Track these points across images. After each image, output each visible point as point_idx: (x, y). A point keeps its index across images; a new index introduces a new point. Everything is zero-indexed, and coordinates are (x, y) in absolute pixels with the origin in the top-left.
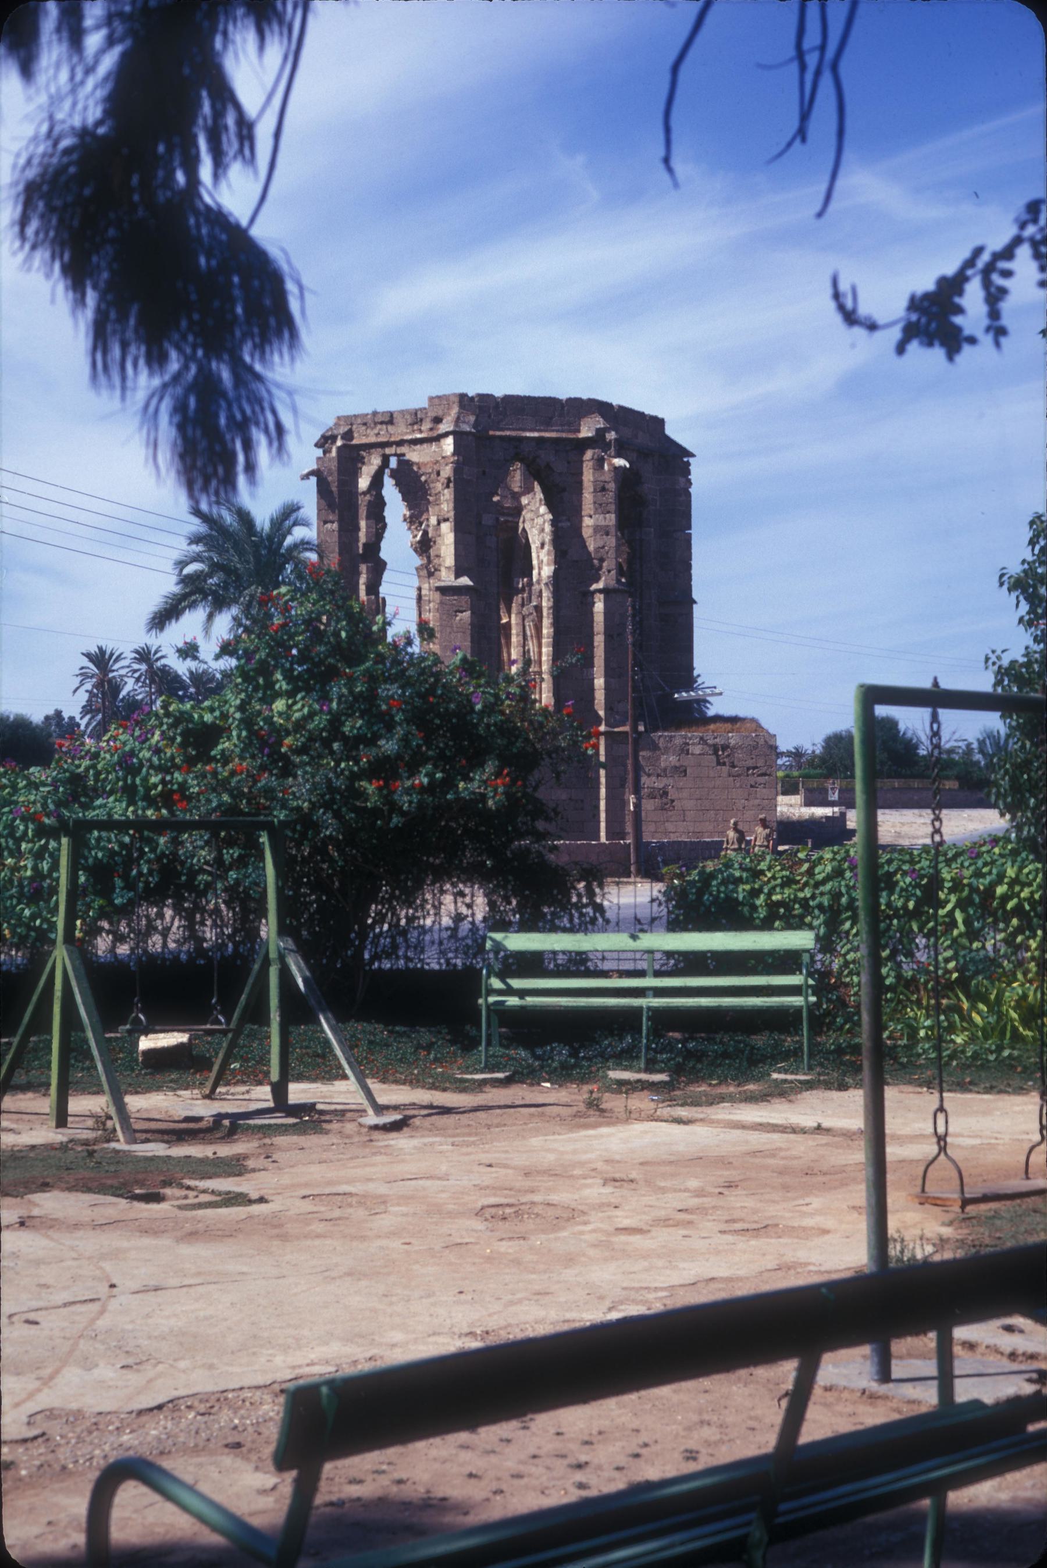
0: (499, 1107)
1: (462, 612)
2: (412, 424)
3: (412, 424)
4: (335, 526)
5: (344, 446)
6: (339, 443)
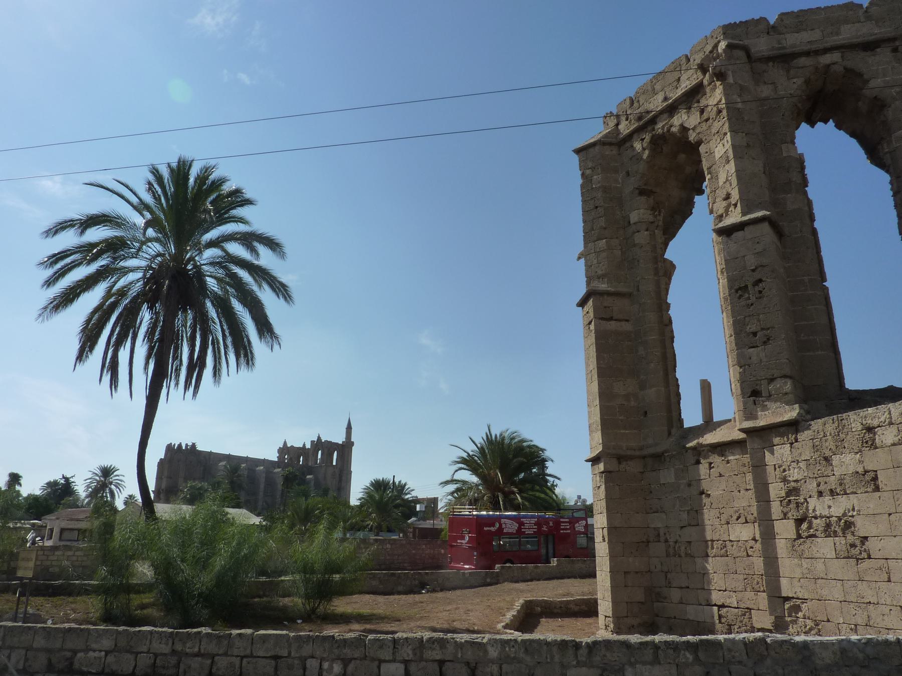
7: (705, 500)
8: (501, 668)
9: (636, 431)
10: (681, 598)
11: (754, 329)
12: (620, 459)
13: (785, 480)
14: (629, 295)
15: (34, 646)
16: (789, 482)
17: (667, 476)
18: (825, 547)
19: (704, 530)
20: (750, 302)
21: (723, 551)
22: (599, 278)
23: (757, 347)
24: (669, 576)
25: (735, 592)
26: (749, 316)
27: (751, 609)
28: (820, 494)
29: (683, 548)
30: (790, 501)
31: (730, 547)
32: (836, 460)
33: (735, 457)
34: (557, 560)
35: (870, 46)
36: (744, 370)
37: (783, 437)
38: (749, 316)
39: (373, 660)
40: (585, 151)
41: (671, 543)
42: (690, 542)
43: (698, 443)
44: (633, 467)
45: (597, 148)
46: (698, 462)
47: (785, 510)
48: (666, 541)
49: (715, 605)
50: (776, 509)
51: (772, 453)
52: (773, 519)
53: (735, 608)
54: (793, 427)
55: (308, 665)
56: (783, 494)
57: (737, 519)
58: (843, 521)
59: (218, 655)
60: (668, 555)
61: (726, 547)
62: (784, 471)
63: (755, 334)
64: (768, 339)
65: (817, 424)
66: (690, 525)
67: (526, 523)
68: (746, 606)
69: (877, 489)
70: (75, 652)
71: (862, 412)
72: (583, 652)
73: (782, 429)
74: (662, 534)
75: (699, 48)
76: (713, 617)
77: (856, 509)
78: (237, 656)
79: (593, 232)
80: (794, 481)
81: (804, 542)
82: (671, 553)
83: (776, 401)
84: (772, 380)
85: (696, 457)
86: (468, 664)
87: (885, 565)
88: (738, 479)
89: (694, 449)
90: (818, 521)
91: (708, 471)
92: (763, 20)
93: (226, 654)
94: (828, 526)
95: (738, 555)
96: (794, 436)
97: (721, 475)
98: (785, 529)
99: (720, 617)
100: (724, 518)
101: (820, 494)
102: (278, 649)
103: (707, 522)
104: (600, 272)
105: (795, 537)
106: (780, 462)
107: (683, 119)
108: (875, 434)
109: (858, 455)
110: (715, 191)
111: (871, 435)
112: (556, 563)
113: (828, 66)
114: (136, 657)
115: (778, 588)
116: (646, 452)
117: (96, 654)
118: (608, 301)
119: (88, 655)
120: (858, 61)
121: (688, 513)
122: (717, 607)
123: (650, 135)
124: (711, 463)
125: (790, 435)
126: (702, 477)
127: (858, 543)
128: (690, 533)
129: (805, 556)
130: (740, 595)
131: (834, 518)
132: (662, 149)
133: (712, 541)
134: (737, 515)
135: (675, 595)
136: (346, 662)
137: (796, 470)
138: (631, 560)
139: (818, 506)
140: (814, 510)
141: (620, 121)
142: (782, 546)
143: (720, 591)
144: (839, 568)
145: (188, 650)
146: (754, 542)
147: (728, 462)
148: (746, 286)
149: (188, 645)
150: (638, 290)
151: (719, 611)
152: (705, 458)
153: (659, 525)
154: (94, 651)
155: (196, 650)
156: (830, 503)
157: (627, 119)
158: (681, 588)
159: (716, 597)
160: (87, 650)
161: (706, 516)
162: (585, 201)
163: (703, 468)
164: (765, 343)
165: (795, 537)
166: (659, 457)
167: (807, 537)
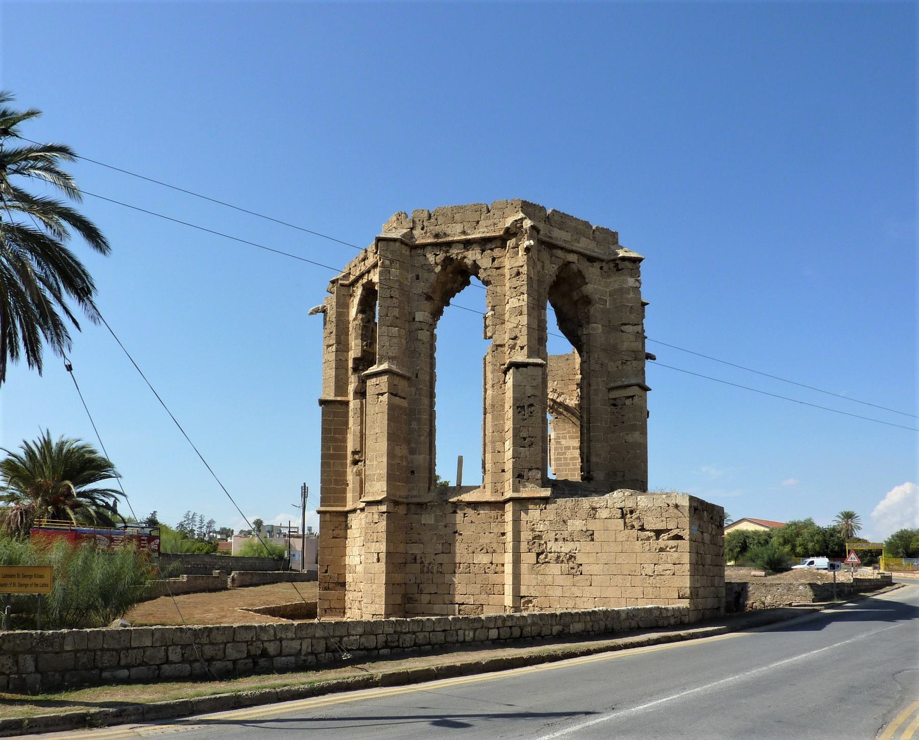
7: (458, 537)
8: (531, 628)
9: (404, 484)
10: (430, 600)
11: (525, 436)
12: (396, 503)
13: (533, 530)
14: (408, 379)
15: (317, 636)
16: (535, 531)
17: (428, 519)
19: (455, 557)
20: (524, 417)
21: (467, 570)
22: (389, 359)
23: (525, 447)
24: (421, 586)
25: (473, 595)
26: (523, 426)
27: (483, 605)
28: (556, 540)
29: (435, 568)
30: (535, 542)
31: (473, 567)
32: (570, 522)
33: (485, 512)
34: (187, 577)
35: (591, 259)
36: (516, 461)
37: (536, 505)
38: (523, 426)
39: (486, 628)
40: (386, 242)
41: (425, 565)
42: (442, 564)
43: (458, 500)
44: (402, 510)
45: (398, 244)
46: (455, 512)
47: (530, 547)
48: (422, 563)
49: (457, 604)
50: (524, 546)
51: (527, 514)
52: (521, 552)
53: (472, 605)
54: (545, 500)
55: (459, 634)
56: (531, 538)
57: (481, 551)
58: (568, 555)
59: (418, 632)
60: (422, 572)
61: (469, 567)
62: (534, 525)
63: (525, 439)
64: (532, 444)
65: (561, 501)
67: (116, 540)
68: (480, 603)
69: (592, 540)
70: (341, 637)
71: (590, 499)
72: (558, 618)
74: (418, 558)
75: (500, 207)
76: (454, 611)
77: (578, 549)
78: (427, 632)
79: (387, 318)
80: (539, 531)
81: (540, 566)
82: (425, 571)
83: (531, 483)
84: (530, 470)
85: (454, 509)
86: (520, 627)
87: (590, 578)
88: (485, 526)
89: (453, 503)
90: (552, 554)
91: (463, 518)
92: (543, 209)
93: (422, 631)
94: (558, 557)
95: (479, 572)
96: (544, 506)
97: (472, 522)
98: (528, 559)
99: (459, 610)
100: (471, 550)
101: (556, 540)
102: (445, 626)
103: (457, 551)
104: (390, 354)
105: (535, 563)
106: (532, 520)
108: (596, 511)
109: (584, 521)
110: (496, 325)
111: (594, 512)
112: (186, 579)
113: (570, 262)
114: (376, 637)
115: (519, 591)
116: (411, 500)
117: (355, 637)
118: (397, 380)
119: (350, 639)
120: (585, 267)
121: (442, 545)
122: (458, 605)
123: (444, 255)
124: (465, 514)
125: (541, 505)
127: (576, 567)
128: (444, 558)
129: (540, 573)
130: (476, 597)
131: (562, 553)
132: (446, 268)
134: (481, 548)
135: (425, 598)
136: (475, 630)
137: (542, 525)
138: (396, 575)
139: (552, 546)
140: (551, 549)
141: (415, 227)
142: (524, 568)
143: (462, 595)
144: (560, 580)
145: (404, 631)
146: (491, 565)
147: (479, 514)
148: (524, 406)
149: (403, 627)
150: (417, 377)
151: (459, 606)
154: (353, 635)
155: (407, 630)
156: (562, 545)
157: (423, 229)
158: (431, 594)
159: (458, 599)
160: (349, 635)
161: (457, 548)
162: (382, 288)
163: (459, 515)
164: (530, 446)
165: (535, 563)
166: (421, 505)
167: (543, 564)
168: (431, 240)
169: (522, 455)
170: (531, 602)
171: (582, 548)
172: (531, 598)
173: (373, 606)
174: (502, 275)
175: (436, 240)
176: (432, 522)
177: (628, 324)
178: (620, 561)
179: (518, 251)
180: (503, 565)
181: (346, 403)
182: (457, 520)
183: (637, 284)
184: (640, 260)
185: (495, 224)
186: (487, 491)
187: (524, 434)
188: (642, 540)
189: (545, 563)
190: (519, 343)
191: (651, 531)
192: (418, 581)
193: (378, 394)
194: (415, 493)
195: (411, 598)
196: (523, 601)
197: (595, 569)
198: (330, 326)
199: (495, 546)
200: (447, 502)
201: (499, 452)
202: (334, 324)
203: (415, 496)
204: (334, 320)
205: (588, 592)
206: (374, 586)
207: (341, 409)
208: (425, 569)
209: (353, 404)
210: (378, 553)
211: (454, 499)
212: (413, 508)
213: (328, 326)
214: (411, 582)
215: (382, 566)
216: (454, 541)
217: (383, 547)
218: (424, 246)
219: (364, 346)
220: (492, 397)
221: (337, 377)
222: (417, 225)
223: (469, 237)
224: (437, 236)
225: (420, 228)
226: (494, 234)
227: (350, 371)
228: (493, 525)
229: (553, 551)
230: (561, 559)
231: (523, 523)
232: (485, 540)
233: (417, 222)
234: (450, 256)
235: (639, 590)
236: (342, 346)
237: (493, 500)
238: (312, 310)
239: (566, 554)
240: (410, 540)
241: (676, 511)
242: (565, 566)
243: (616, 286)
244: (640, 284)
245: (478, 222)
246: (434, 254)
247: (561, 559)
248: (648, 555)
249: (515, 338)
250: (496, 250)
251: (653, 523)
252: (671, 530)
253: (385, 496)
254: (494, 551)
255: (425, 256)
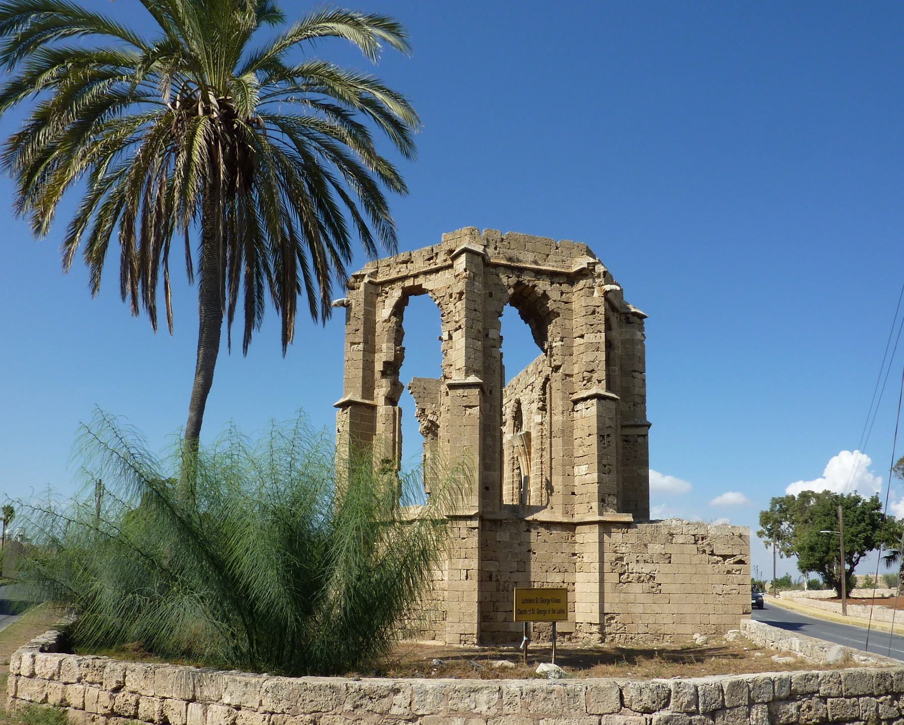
0: (153, 102)
1: (470, 407)
2: (429, 259)
3: (429, 259)
4: (361, 346)
5: (370, 282)
6: (366, 280)
7: (533, 556)
18: (637, 588)
19: (530, 575)
28: (638, 561)
46: (529, 531)
47: (613, 568)
48: (497, 580)
50: (607, 567)
51: (610, 537)
54: (628, 525)
56: (614, 559)
60: (498, 590)
62: (616, 547)
63: (605, 466)
66: (518, 571)
73: (619, 525)
74: (494, 576)
75: (568, 246)
82: (501, 589)
84: (609, 495)
90: (634, 575)
94: (640, 577)
98: (611, 578)
99: (534, 628)
103: (532, 570)
104: (475, 367)
107: (553, 291)
126: (532, 541)
127: (656, 586)
133: (534, 582)
142: (608, 587)
144: (642, 598)
147: (551, 534)
152: (535, 528)
153: (493, 570)
156: (644, 566)
158: (506, 612)
161: (532, 566)
163: (533, 533)
168: (504, 262)
169: (604, 481)
170: (613, 618)
171: (661, 570)
172: (614, 615)
173: (461, 625)
174: (569, 310)
175: (509, 263)
176: (508, 540)
177: (637, 372)
178: (694, 581)
179: (594, 292)
180: (574, 584)
181: (374, 408)
182: (532, 538)
183: (642, 338)
184: (645, 317)
185: (563, 261)
186: (556, 511)
187: (605, 462)
188: (712, 563)
189: (627, 582)
190: (595, 376)
191: (718, 556)
192: (494, 599)
193: (466, 407)
194: (490, 509)
195: (486, 616)
196: (606, 617)
197: (673, 588)
198: (355, 323)
199: (566, 565)
200: (522, 520)
201: (569, 475)
202: (361, 322)
203: (490, 513)
204: (362, 317)
205: (667, 608)
206: (462, 605)
207: (367, 413)
208: (501, 588)
209: (383, 409)
210: (467, 570)
211: (530, 518)
212: (487, 523)
213: (353, 322)
214: (487, 600)
215: (474, 584)
216: (529, 560)
217: (474, 564)
218: (497, 266)
219: (398, 351)
220: (563, 423)
221: (364, 377)
222: (490, 244)
223: (541, 267)
224: (510, 259)
225: (493, 247)
226: (563, 270)
227: (378, 375)
228: (564, 545)
229: (634, 571)
230: (642, 579)
231: (606, 545)
232: (558, 559)
233: (491, 241)
234: (522, 281)
235: (711, 607)
236: (370, 348)
237: (566, 521)
238: (338, 302)
239: (647, 574)
240: (486, 557)
241: (739, 539)
242: (646, 586)
243: (628, 337)
244: (645, 338)
245: (548, 255)
246: (507, 276)
247: (642, 579)
248: (718, 576)
249: (592, 371)
250: (564, 286)
251: (721, 549)
252: (736, 555)
253: (477, 511)
254: (566, 571)
255: (498, 276)
